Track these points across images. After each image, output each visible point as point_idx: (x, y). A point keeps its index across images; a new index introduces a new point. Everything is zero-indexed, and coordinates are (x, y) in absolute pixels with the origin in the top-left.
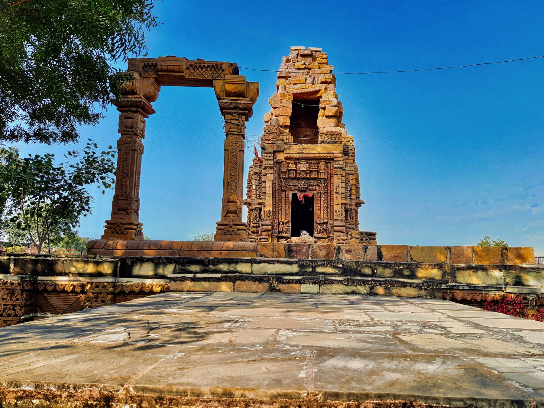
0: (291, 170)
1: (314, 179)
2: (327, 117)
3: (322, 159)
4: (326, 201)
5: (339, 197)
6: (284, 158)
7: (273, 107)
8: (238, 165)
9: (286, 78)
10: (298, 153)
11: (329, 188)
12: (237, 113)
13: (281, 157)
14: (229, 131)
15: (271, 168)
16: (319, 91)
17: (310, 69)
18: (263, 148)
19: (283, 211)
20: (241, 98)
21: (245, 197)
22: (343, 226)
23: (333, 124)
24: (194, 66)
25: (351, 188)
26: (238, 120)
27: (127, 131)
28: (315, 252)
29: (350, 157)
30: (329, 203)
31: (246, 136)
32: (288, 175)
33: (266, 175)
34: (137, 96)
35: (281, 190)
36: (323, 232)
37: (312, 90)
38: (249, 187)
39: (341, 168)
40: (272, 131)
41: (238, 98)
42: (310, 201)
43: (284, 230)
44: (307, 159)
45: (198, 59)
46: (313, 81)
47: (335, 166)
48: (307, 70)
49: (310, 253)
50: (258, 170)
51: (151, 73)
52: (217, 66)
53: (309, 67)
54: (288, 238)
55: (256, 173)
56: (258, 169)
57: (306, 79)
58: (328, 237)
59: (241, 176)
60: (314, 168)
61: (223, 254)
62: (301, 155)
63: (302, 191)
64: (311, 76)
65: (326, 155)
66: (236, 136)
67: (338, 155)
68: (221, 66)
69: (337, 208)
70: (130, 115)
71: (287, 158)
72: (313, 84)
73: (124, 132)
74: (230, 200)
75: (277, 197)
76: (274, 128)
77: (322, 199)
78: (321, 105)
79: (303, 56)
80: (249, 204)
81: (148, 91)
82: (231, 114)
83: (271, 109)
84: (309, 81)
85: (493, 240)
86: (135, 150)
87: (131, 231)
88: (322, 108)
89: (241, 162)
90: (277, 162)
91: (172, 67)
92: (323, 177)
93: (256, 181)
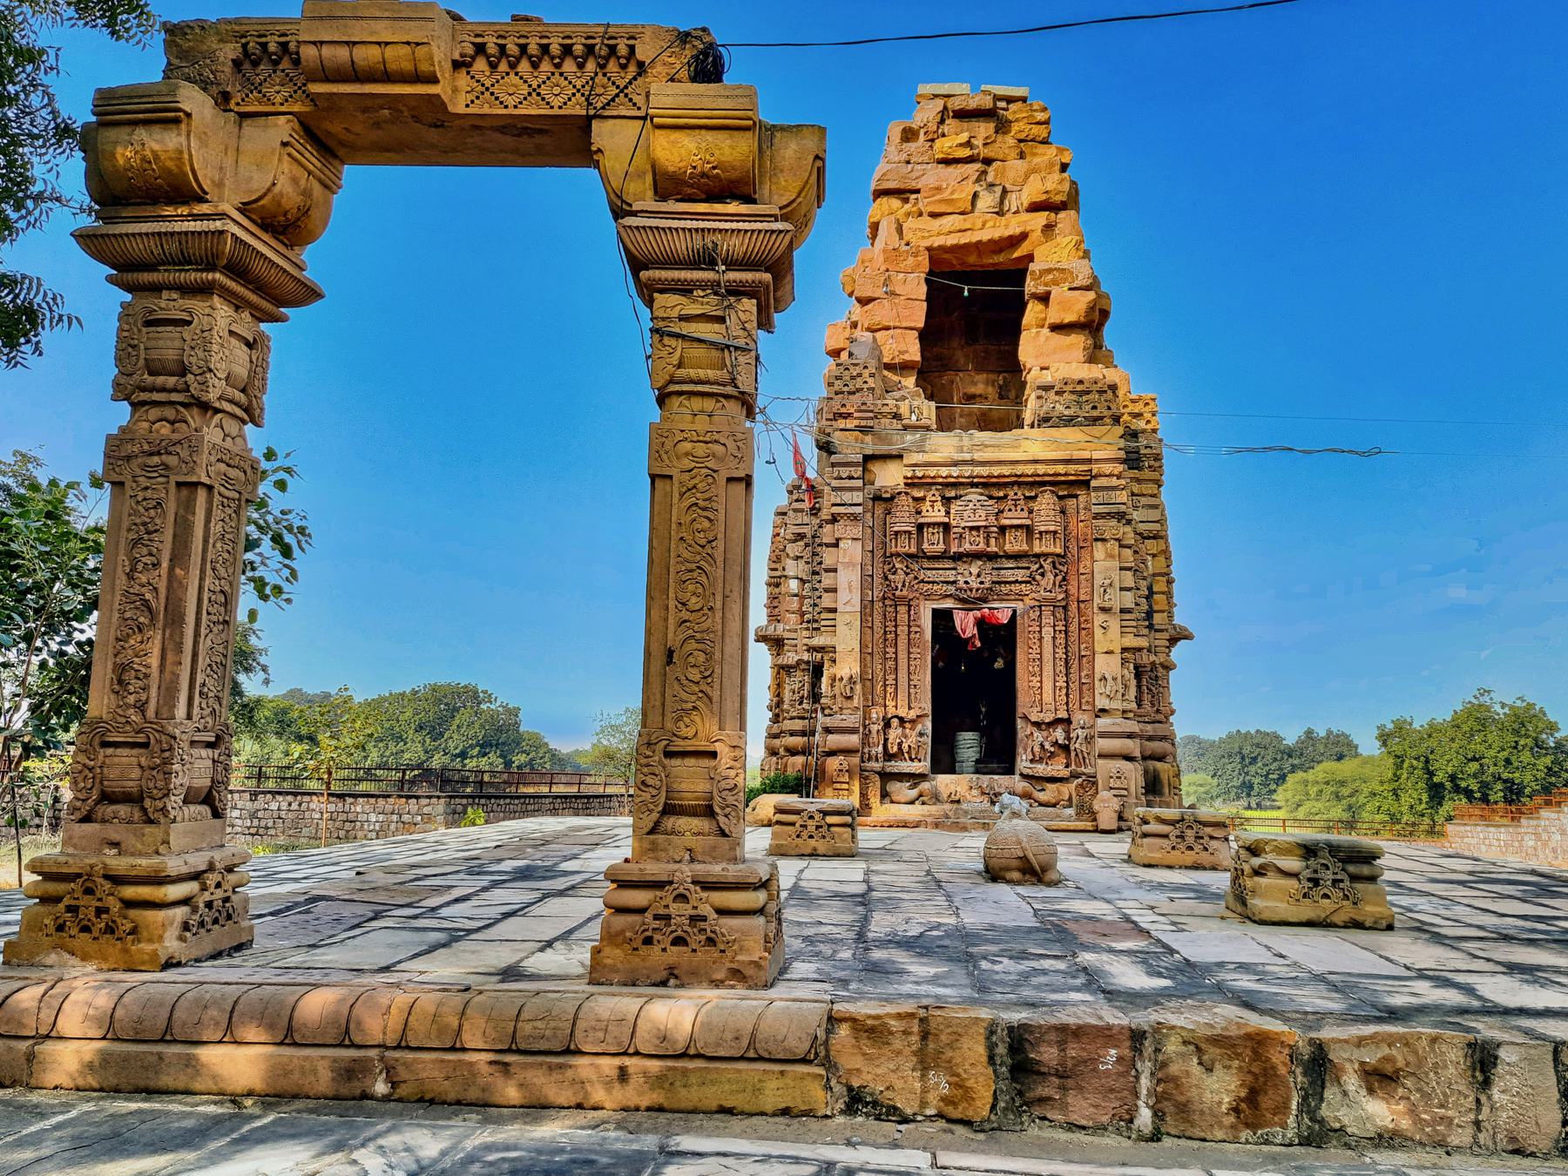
0: (929, 525)
2: (1057, 328)
3: (1044, 484)
5: (1114, 624)
6: (902, 481)
7: (859, 300)
8: (720, 560)
9: (902, 193)
10: (955, 464)
11: (1073, 590)
12: (714, 287)
13: (890, 477)
14: (671, 382)
15: (854, 518)
16: (1024, 236)
17: (988, 162)
18: (825, 447)
19: (903, 675)
20: (733, 207)
21: (758, 617)
22: (1130, 736)
23: (1079, 354)
24: (492, 49)
25: (1150, 588)
26: (721, 320)
27: (153, 389)
28: (1174, 1080)
29: (1147, 474)
30: (1074, 648)
31: (761, 402)
32: (920, 542)
33: (836, 545)
34: (204, 208)
35: (893, 600)
36: (1052, 755)
37: (997, 234)
38: (775, 583)
39: (1121, 516)
40: (859, 383)
41: (719, 208)
42: (1001, 637)
43: (905, 748)
44: (986, 484)
45: (515, 18)
46: (1002, 202)
47: (1095, 509)
48: (978, 166)
49: (1145, 1083)
50: (809, 524)
51: (278, 92)
52: (613, 49)
53: (985, 152)
54: (922, 777)
55: (800, 537)
56: (806, 520)
57: (975, 196)
58: (1075, 776)
59: (736, 608)
61: (636, 1080)
62: (967, 471)
63: (968, 603)
65: (1061, 469)
66: (709, 404)
67: (1107, 468)
68: (632, 48)
69: (1107, 665)
70: (170, 305)
71: (911, 483)
72: (1000, 213)
73: (144, 396)
74: (680, 745)
75: (877, 624)
76: (866, 373)
77: (1048, 632)
78: (1030, 286)
79: (963, 115)
80: (777, 644)
81: (260, 182)
82: (685, 289)
83: (855, 294)
84: (987, 201)
85: (1504, 697)
86: (196, 485)
87: (161, 915)
88: (1036, 297)
89: (736, 536)
90: (877, 498)
91: (375, 52)
92: (1052, 549)
93: (801, 563)
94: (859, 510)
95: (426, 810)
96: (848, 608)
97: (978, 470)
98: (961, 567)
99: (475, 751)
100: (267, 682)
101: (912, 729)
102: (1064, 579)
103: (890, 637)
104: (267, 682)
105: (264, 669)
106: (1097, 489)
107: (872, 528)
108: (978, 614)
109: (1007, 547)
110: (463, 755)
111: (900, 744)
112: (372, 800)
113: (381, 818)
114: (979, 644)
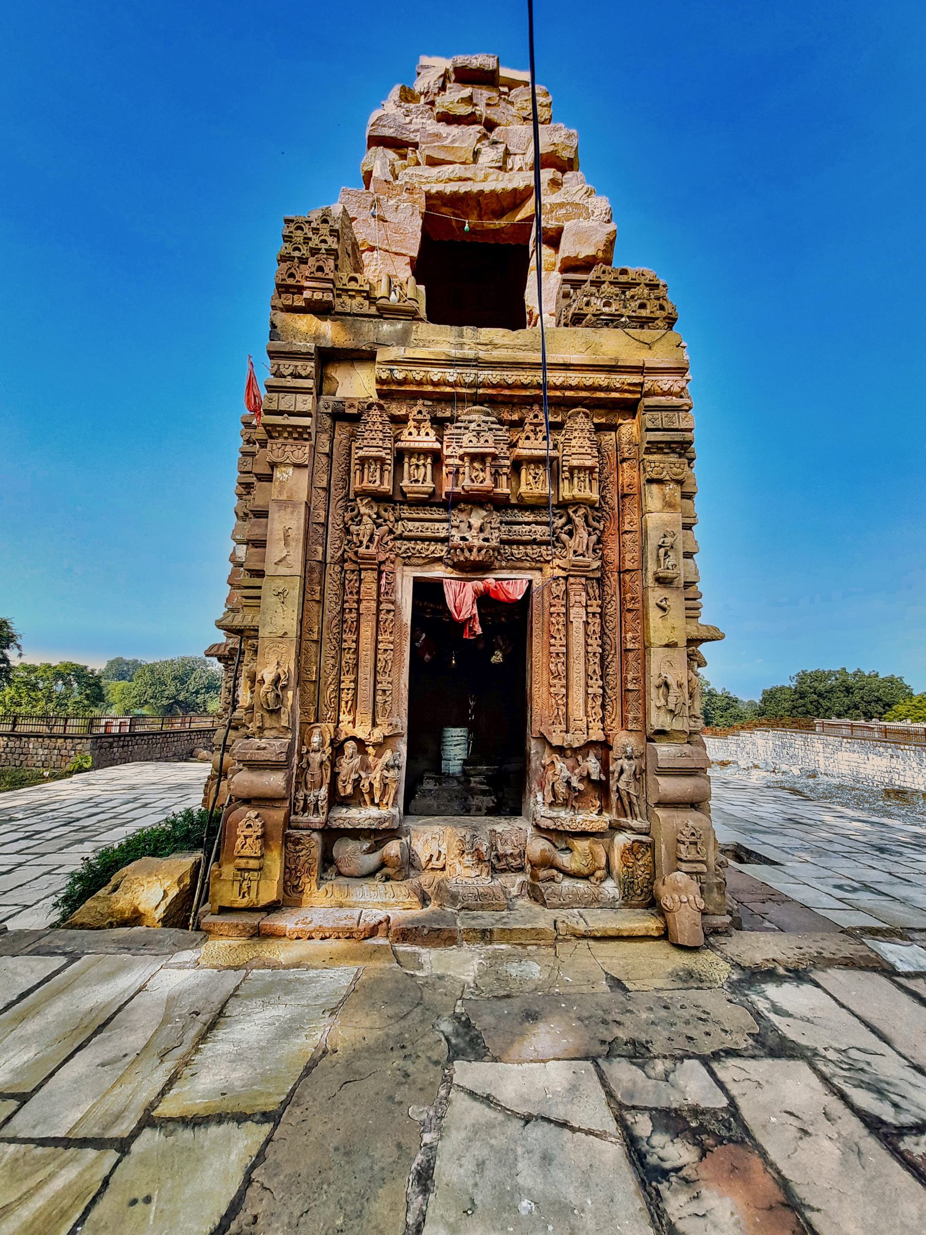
0: (412, 452)
1: (536, 506)
4: (595, 627)
11: (613, 556)
15: (300, 434)
19: (366, 673)
33: (269, 478)
42: (509, 620)
44: (496, 400)
60: (532, 446)
62: (469, 375)
63: (471, 568)
64: (495, 143)
75: (330, 596)
77: (578, 615)
84: (489, 155)
94: (306, 421)
95: (79, 747)
96: (282, 570)
97: (486, 375)
98: (457, 517)
99: (203, 691)
100: (20, 655)
101: (378, 755)
102: (599, 541)
103: (350, 617)
104: (20, 655)
105: (19, 647)
106: (649, 409)
107: (329, 456)
108: (480, 585)
109: (523, 489)
110: (197, 692)
111: (357, 782)
112: (40, 740)
113: (46, 751)
114: (479, 630)
